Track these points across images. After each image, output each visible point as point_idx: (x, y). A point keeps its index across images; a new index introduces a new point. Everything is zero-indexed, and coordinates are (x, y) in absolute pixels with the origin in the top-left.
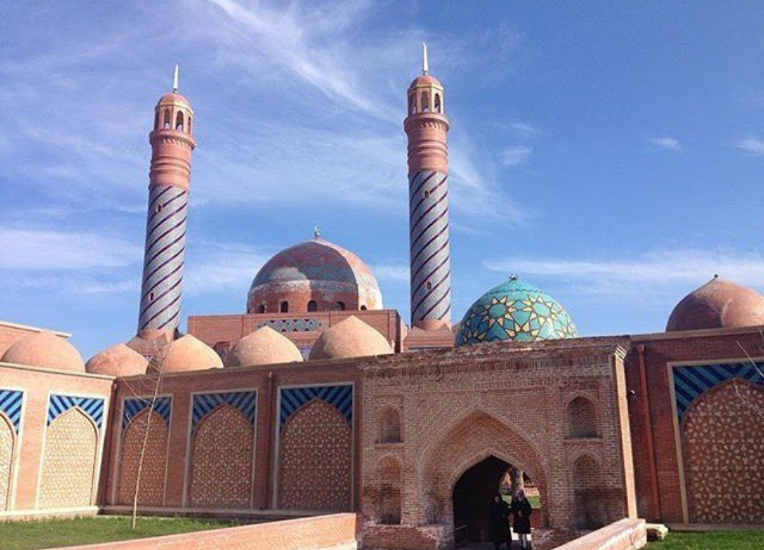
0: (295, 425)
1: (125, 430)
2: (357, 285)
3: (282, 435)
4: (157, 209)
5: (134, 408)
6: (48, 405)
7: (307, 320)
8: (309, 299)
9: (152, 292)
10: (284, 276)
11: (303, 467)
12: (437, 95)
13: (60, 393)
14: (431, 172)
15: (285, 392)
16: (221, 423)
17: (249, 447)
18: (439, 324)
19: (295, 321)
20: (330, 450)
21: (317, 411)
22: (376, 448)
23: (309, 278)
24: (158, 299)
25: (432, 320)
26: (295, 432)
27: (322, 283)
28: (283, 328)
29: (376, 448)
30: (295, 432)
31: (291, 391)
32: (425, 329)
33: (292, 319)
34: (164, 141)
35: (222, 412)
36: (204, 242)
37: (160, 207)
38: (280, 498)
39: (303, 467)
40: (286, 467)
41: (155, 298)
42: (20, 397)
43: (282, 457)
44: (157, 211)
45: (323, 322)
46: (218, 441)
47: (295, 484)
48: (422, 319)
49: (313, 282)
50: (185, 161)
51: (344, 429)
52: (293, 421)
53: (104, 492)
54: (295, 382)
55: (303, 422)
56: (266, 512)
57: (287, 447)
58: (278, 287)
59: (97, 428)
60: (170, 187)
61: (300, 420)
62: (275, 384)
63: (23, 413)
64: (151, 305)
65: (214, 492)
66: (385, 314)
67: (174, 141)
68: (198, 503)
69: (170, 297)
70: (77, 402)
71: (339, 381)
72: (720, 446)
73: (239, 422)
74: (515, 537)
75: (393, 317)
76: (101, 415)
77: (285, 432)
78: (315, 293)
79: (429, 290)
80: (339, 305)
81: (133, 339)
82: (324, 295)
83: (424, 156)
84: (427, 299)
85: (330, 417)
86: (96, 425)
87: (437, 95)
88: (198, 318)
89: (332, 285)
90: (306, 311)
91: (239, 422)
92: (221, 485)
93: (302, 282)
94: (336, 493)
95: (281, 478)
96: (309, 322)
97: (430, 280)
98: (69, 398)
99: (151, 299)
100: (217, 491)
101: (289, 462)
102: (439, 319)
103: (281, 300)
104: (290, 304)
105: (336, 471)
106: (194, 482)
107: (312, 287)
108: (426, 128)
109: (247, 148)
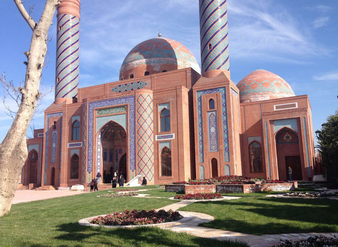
2: (176, 59)
7: (138, 82)
8: (146, 70)
9: (59, 77)
10: (132, 59)
18: (218, 72)
19: (132, 84)
23: (145, 58)
25: (213, 70)
27: (152, 60)
28: (126, 89)
33: (136, 81)
45: (147, 82)
49: (147, 59)
53: (56, 174)
60: (65, 15)
64: (59, 83)
75: (189, 72)
78: (149, 66)
81: (52, 104)
82: (154, 67)
84: (209, 56)
89: (159, 60)
90: (144, 76)
93: (140, 61)
96: (139, 83)
97: (211, 42)
99: (59, 81)
102: (218, 68)
103: (130, 74)
104: (134, 76)
107: (147, 63)
109: (189, 40)
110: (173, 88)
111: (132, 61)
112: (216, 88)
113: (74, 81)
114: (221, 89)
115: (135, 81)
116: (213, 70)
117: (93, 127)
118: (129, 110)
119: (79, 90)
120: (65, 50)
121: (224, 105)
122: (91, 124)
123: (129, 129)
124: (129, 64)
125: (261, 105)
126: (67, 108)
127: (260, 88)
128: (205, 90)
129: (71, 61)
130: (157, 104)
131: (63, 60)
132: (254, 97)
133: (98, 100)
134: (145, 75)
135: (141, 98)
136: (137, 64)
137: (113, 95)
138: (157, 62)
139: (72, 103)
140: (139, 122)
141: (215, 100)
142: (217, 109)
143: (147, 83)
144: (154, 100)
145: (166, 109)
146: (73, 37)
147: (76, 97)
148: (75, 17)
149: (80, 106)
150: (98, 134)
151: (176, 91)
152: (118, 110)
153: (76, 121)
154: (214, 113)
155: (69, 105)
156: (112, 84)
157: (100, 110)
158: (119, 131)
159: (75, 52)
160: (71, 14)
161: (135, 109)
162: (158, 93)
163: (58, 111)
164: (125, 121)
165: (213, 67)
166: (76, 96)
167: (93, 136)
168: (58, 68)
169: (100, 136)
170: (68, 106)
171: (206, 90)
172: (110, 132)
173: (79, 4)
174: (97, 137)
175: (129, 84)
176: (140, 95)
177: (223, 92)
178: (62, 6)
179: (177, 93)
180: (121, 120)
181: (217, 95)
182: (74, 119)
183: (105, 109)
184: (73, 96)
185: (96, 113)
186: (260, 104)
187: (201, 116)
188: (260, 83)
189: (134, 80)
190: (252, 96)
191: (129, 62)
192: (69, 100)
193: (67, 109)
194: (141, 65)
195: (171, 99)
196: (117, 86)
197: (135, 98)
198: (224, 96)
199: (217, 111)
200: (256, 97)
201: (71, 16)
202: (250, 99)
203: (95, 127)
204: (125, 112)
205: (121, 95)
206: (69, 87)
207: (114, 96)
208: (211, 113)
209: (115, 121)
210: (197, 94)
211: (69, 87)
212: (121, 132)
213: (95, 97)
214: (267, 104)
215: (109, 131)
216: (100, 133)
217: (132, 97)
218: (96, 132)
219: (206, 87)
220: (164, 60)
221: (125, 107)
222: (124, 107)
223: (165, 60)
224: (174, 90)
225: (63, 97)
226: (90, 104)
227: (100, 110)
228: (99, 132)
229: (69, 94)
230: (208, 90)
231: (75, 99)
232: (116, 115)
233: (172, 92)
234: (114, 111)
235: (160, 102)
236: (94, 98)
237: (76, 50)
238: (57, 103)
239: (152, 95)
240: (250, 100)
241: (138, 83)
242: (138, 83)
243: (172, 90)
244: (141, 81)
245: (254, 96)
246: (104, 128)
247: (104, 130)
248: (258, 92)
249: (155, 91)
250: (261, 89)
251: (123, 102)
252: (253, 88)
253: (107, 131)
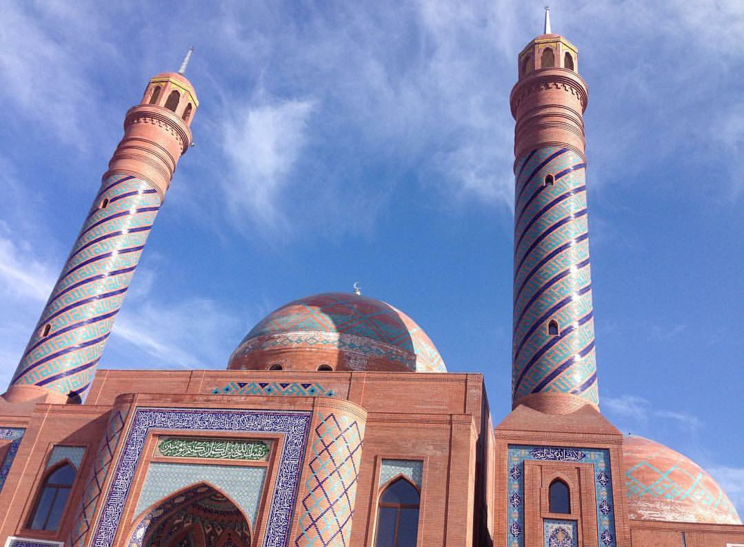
4: (102, 204)
10: (284, 326)
12: (567, 54)
14: (558, 149)
19: (284, 386)
24: (55, 334)
32: (542, 411)
34: (141, 120)
36: (311, 449)
37: (106, 203)
41: (51, 332)
44: (100, 207)
48: (537, 390)
50: (169, 154)
58: (271, 342)
60: (131, 177)
66: (459, 380)
69: (82, 335)
74: (355, 285)
75: (476, 387)
79: (553, 336)
82: (350, 358)
83: (544, 127)
87: (567, 54)
90: (316, 370)
93: (312, 333)
97: (556, 317)
99: (46, 334)
108: (550, 91)
110: (441, 418)
111: (284, 330)
112: (578, 449)
113: (91, 346)
114: (593, 453)
115: (295, 381)
116: (561, 394)
117: (127, 494)
118: (279, 456)
119: (100, 373)
120: (99, 258)
121: (606, 507)
122: (122, 482)
123: (265, 522)
124: (276, 336)
125: (686, 535)
126: (46, 415)
127: (666, 486)
128: (537, 448)
129: (100, 292)
130: (376, 458)
131: (83, 282)
132: (648, 508)
133: (174, 405)
134: (318, 370)
135: (330, 425)
136: (301, 341)
137: (234, 398)
138: (360, 347)
139: (64, 402)
140: (308, 505)
141: (573, 486)
142: (579, 518)
143: (333, 393)
144: (366, 443)
145: (408, 481)
146: (132, 234)
147: (80, 394)
148: (154, 191)
149: (96, 416)
150: (139, 522)
151: (449, 427)
152: (239, 450)
153: (66, 463)
154: (569, 528)
155: (56, 409)
156: (218, 377)
157: (173, 438)
158: (208, 531)
159: (125, 271)
160: (148, 180)
161: (302, 457)
162: (385, 424)
163: (11, 422)
164: (256, 495)
165: (563, 384)
166: (81, 390)
167: (117, 530)
168: (57, 301)
169: (141, 533)
170: (53, 411)
171: (543, 447)
172: (179, 525)
173: (173, 170)
174: (131, 533)
175: (275, 384)
176: (328, 414)
177: (602, 465)
178: (131, 158)
179: (451, 436)
180: (241, 487)
181: (578, 469)
182: (58, 458)
183: (189, 439)
184: (74, 390)
185: (154, 448)
186: (683, 533)
187: (521, 529)
188: (664, 472)
189: (291, 378)
190: (643, 505)
191: (275, 332)
192: (57, 394)
193: (48, 419)
194: (313, 346)
195: (427, 451)
196: (232, 384)
197: (309, 423)
198: (603, 478)
199: (579, 522)
200: (655, 509)
201: (144, 186)
202: (639, 512)
203: (137, 495)
204: (263, 460)
205: (260, 404)
206: (68, 362)
207: (237, 403)
208: (556, 526)
209: (218, 487)
210: (510, 453)
211: (68, 362)
212: (212, 533)
213: (167, 395)
214: (706, 535)
215: (177, 521)
216: (148, 522)
217: (301, 417)
218: (136, 513)
219: (541, 439)
220: (379, 349)
221: (268, 444)
222: (262, 443)
223: (381, 347)
224: (441, 422)
225: (40, 384)
226: (142, 416)
227: (173, 438)
228: (145, 515)
229: (60, 380)
230: (547, 447)
231: (74, 397)
232: (226, 466)
233: (433, 429)
234: (221, 452)
235: (388, 451)
236: (162, 395)
237: (128, 267)
238: (11, 398)
239: (362, 426)
240: (636, 513)
241: (306, 388)
242: (306, 388)
243: (436, 422)
244: (317, 384)
245: (650, 505)
246: (168, 506)
247: (164, 514)
248: (660, 497)
249: (374, 416)
250: (670, 489)
251: (264, 428)
252: (645, 481)
253: (170, 518)
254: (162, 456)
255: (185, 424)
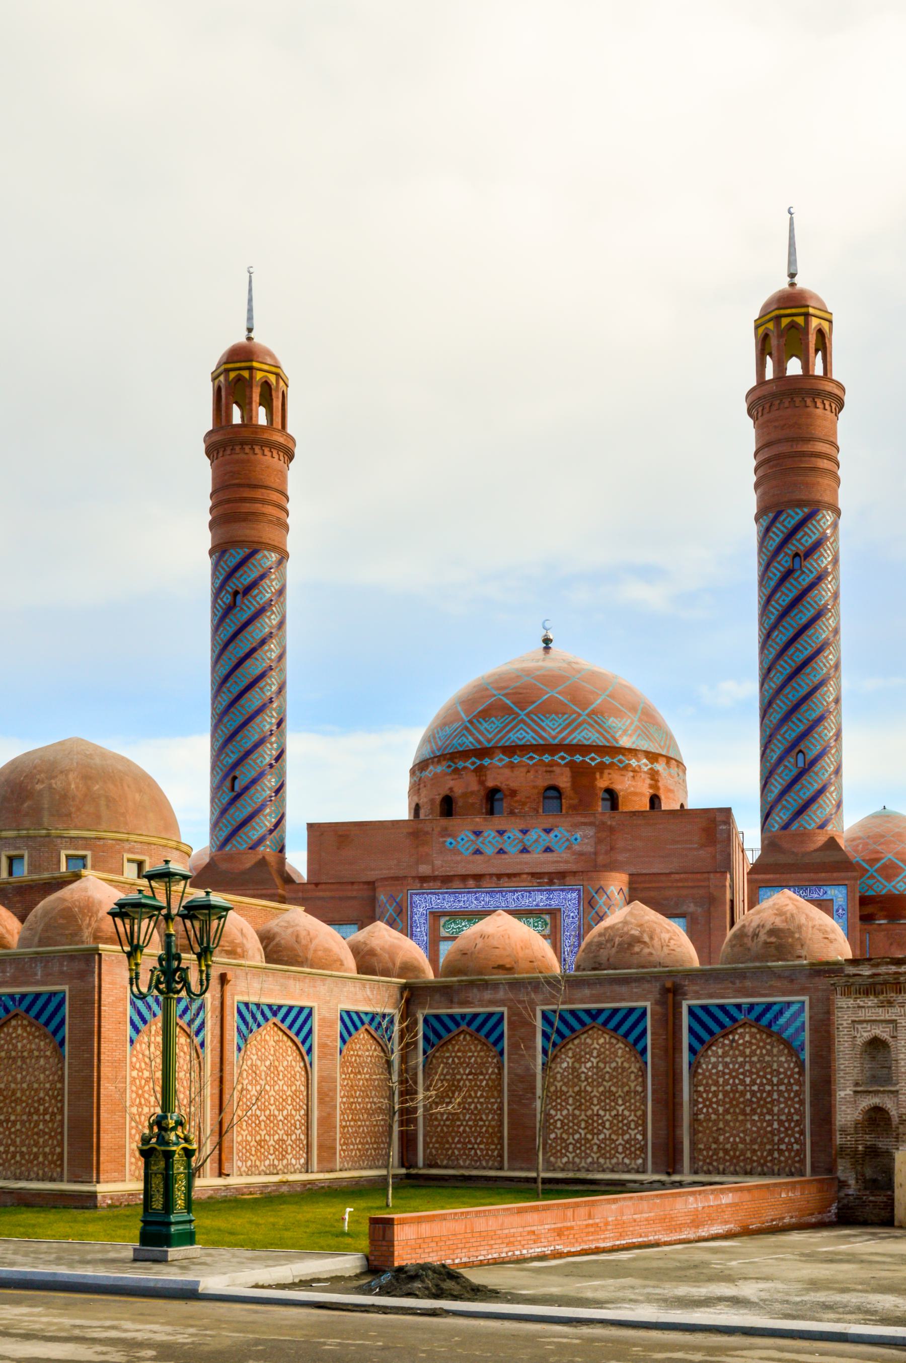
0: (715, 1057)
1: (242, 1052)
3: (693, 1073)
5: (440, 1032)
6: (339, 1026)
11: (728, 1117)
13: (253, 999)
15: (694, 1009)
16: (591, 1054)
17: (639, 1089)
20: (770, 1093)
21: (747, 1038)
22: (855, 1092)
26: (713, 1068)
29: (855, 1092)
30: (713, 1068)
31: (704, 1008)
35: (589, 1037)
38: (693, 1159)
39: (728, 1117)
40: (701, 1117)
42: (310, 1014)
43: (694, 1103)
46: (586, 1079)
47: (716, 1141)
51: (792, 1065)
52: (710, 1053)
54: (711, 996)
55: (725, 1054)
56: (676, 1178)
57: (701, 1089)
59: (199, 1048)
61: (720, 1051)
62: (678, 998)
63: (316, 1038)
65: (585, 1151)
67: (267, 451)
68: (561, 1166)
70: (366, 1019)
71: (784, 995)
72: (715, 1094)
73: (620, 1051)
76: (202, 1025)
77: (697, 1067)
80: (607, 796)
85: (768, 1047)
86: (304, 1050)
88: (319, 825)
91: (620, 1051)
92: (596, 1141)
94: (781, 1152)
95: (694, 1132)
98: (357, 1013)
100: (591, 1148)
101: (705, 1110)
105: (781, 1123)
106: (553, 1136)
254: (448, 935)
255: (462, 904)
